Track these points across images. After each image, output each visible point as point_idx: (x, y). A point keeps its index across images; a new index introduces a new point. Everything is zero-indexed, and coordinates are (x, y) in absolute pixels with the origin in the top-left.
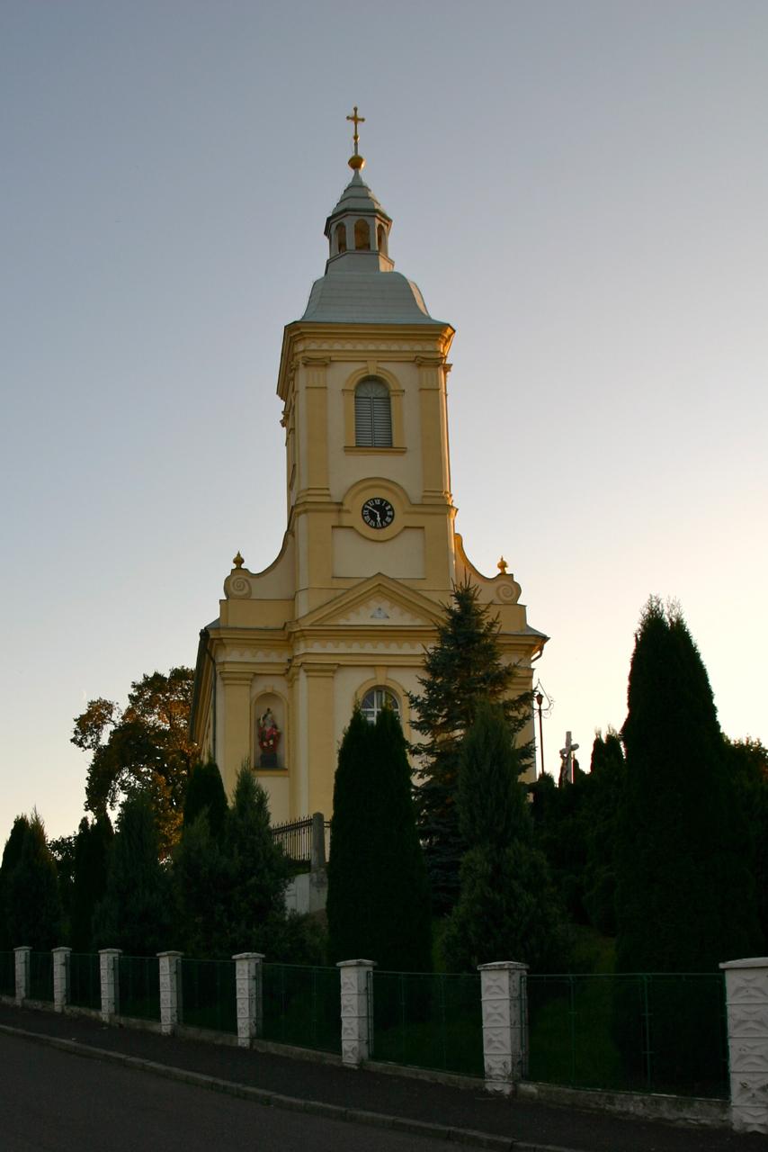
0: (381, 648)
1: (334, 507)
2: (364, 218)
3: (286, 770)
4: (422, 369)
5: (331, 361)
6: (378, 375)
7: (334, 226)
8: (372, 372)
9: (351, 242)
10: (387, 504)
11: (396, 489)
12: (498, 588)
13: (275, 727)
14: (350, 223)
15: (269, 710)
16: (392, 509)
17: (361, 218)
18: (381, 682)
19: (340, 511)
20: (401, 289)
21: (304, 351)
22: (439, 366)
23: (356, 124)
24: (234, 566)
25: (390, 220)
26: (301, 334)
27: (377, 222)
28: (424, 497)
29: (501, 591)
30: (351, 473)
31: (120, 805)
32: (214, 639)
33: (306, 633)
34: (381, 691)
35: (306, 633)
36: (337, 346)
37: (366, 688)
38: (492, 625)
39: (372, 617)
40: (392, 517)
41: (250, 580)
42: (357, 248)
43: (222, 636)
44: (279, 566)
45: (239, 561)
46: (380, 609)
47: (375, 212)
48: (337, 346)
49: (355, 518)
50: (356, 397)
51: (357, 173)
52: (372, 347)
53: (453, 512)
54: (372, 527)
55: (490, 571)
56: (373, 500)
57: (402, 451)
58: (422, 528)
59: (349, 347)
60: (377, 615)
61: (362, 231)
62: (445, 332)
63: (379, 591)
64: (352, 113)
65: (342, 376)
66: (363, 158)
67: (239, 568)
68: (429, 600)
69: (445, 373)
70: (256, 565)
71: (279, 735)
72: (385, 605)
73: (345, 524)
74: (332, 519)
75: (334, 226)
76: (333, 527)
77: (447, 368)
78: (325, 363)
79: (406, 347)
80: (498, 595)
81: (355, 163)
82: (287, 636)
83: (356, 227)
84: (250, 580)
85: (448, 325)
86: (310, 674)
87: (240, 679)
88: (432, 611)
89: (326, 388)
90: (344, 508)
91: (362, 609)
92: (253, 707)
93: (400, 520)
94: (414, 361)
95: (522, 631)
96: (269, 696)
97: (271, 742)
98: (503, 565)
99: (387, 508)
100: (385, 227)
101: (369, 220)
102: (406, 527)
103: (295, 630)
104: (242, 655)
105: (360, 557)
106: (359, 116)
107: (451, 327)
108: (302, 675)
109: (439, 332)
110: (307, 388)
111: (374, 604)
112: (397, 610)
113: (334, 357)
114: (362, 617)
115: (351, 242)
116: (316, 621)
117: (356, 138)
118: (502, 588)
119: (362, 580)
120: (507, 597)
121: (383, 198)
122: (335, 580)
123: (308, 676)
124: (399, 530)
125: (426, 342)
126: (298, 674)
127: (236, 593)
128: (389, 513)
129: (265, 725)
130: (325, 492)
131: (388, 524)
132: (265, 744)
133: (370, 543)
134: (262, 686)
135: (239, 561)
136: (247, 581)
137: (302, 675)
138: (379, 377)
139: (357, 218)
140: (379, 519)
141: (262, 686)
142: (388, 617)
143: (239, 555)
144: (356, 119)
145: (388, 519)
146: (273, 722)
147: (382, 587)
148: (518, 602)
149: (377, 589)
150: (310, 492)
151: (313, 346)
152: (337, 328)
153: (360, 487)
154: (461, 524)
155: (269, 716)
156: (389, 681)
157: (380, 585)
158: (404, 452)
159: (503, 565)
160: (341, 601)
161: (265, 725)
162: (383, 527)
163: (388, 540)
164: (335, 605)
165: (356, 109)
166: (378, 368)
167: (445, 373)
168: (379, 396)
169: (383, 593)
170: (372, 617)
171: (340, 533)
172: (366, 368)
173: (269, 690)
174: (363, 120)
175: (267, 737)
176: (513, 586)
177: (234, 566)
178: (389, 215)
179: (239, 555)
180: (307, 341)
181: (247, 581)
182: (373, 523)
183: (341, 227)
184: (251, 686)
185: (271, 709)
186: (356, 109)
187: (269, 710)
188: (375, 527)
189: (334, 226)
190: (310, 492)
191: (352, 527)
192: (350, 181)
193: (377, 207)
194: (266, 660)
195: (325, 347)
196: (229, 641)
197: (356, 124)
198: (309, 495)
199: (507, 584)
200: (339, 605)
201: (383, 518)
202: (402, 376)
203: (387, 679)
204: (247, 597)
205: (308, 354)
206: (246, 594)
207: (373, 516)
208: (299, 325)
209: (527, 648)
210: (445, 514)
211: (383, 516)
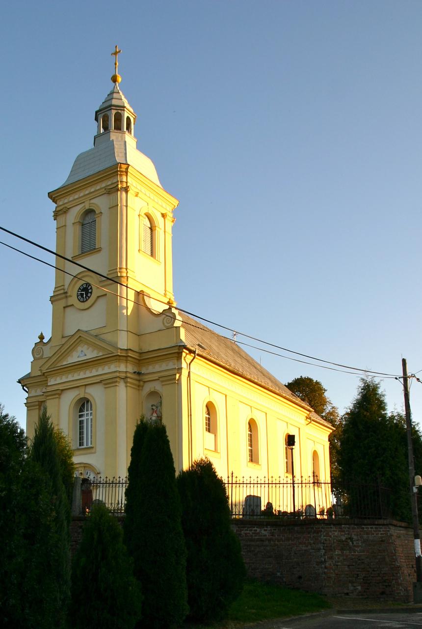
1: (64, 295)
2: (119, 111)
3: (219, 453)
5: (69, 209)
6: (91, 208)
12: (164, 319)
17: (104, 113)
19: (66, 297)
24: (39, 340)
27: (114, 112)
31: (417, 488)
39: (78, 357)
40: (91, 293)
43: (25, 383)
49: (74, 300)
52: (82, 194)
60: (81, 355)
62: (120, 167)
65: (74, 214)
76: (64, 307)
80: (163, 324)
88: (66, 348)
90: (68, 294)
93: (95, 293)
102: (98, 297)
111: (79, 349)
113: (68, 206)
114: (74, 358)
116: (49, 367)
119: (69, 337)
120: (168, 323)
130: (62, 287)
133: (83, 312)
136: (42, 348)
140: (84, 296)
142: (86, 355)
143: (42, 334)
145: (89, 295)
148: (175, 325)
149: (79, 340)
152: (68, 188)
156: (86, 394)
157: (80, 336)
158: (100, 251)
160: (61, 351)
166: (90, 204)
170: (78, 357)
171: (68, 310)
172: (85, 206)
177: (39, 340)
179: (42, 334)
182: (82, 300)
201: (86, 295)
202: (101, 203)
207: (82, 295)
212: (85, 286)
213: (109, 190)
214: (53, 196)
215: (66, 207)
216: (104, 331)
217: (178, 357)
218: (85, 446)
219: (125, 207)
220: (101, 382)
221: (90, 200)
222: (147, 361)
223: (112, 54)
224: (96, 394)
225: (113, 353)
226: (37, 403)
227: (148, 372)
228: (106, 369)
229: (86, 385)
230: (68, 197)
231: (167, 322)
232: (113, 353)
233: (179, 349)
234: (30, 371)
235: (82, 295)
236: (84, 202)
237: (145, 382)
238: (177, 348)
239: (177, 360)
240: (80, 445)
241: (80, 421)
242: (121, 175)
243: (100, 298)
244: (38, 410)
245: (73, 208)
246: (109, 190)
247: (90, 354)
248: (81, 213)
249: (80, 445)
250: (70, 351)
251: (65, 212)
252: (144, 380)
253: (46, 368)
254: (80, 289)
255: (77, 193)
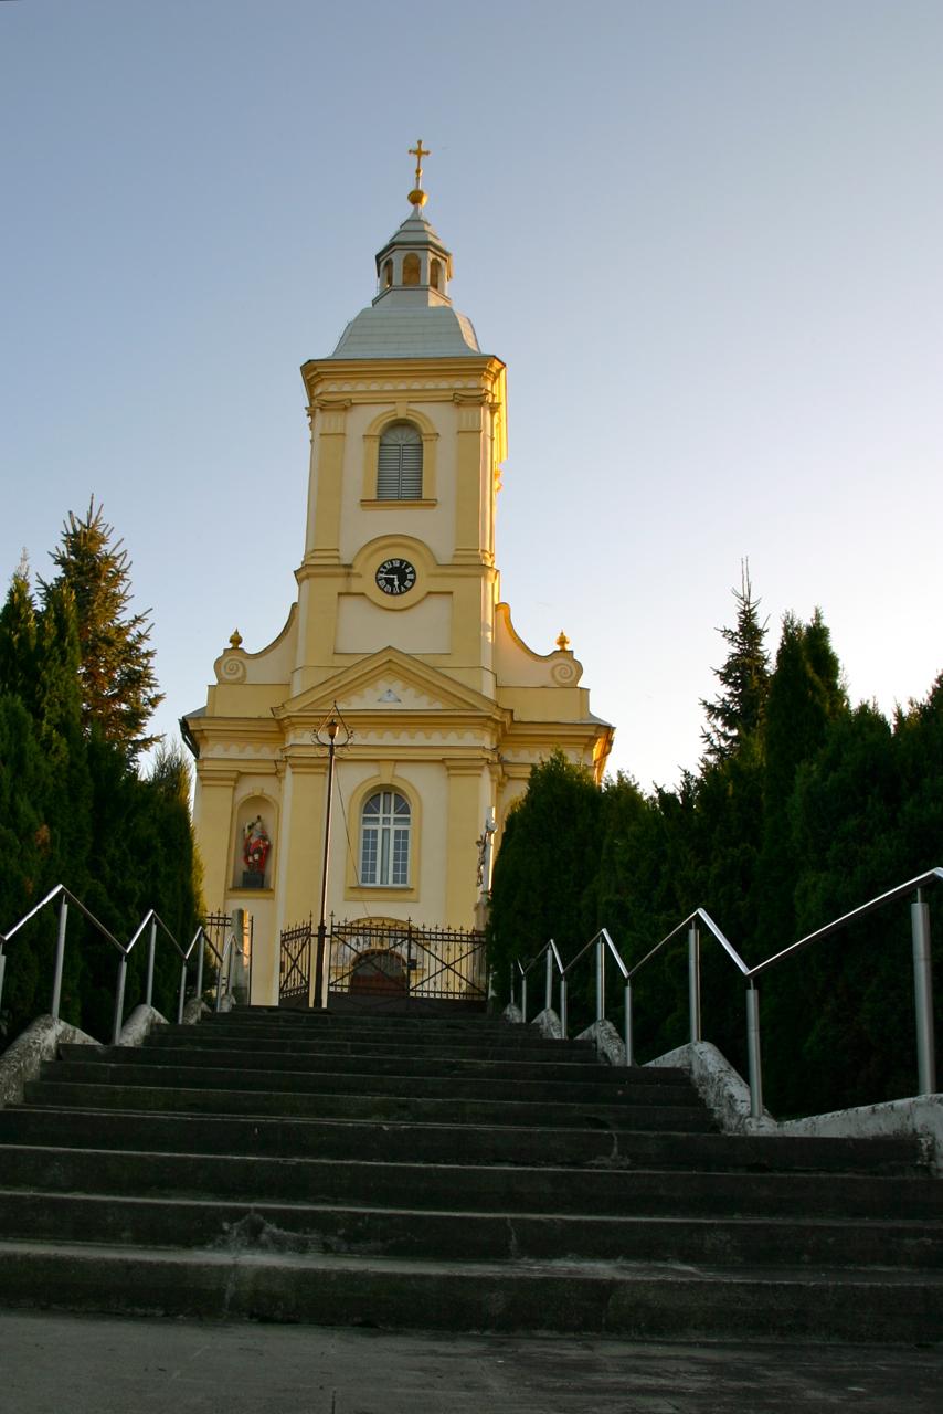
0: (388, 738)
1: (342, 570)
4: (461, 408)
5: (353, 404)
6: (410, 418)
7: (383, 260)
8: (401, 415)
9: (398, 278)
10: (408, 565)
11: (420, 548)
12: (553, 668)
13: (264, 838)
14: (398, 258)
15: (259, 818)
16: (413, 572)
18: (386, 780)
19: (348, 575)
20: (447, 321)
21: (321, 394)
22: (482, 404)
23: (419, 158)
24: (230, 646)
25: (447, 254)
26: (319, 374)
27: (431, 256)
28: (455, 556)
29: (556, 673)
30: (369, 530)
32: (194, 731)
33: (294, 720)
34: (390, 794)
35: (294, 720)
36: (361, 387)
37: (361, 793)
38: (141, 637)
40: (413, 581)
41: (245, 661)
42: (405, 283)
43: (203, 727)
44: (284, 642)
45: (236, 640)
46: (390, 691)
47: (426, 245)
48: (361, 387)
49: (367, 583)
50: (381, 445)
51: (416, 209)
52: (402, 386)
53: (491, 574)
54: (387, 593)
55: (544, 646)
56: (391, 561)
57: (432, 504)
58: (451, 593)
59: (374, 387)
61: (412, 269)
62: (491, 365)
63: (389, 669)
64: (416, 146)
65: (366, 420)
66: (424, 191)
67: (235, 648)
68: (450, 679)
69: (492, 413)
70: (251, 646)
71: (268, 848)
72: (397, 686)
73: (354, 590)
74: (338, 584)
75: (383, 264)
76: (340, 594)
77: (494, 408)
78: (345, 407)
79: (444, 384)
80: (553, 676)
81: (415, 198)
82: (278, 726)
83: (409, 262)
84: (245, 661)
85: (495, 357)
86: (297, 770)
87: (222, 779)
89: (344, 434)
90: (354, 571)
91: (368, 691)
92: (236, 812)
93: (423, 584)
94: (452, 401)
95: (582, 719)
96: (258, 801)
97: (257, 857)
98: (562, 641)
99: (407, 571)
100: (443, 263)
101: (420, 254)
102: (430, 593)
103: (282, 717)
104: (226, 750)
105: (369, 627)
106: (423, 149)
107: (498, 360)
108: (289, 771)
109: (481, 365)
110: (321, 435)
111: (383, 685)
112: (411, 691)
115: (398, 278)
117: (418, 172)
118: (559, 668)
121: (440, 230)
122: (337, 657)
123: (293, 773)
124: (422, 595)
125: (467, 377)
126: (284, 771)
127: (228, 677)
128: (409, 576)
129: (251, 836)
130: (335, 553)
131: (408, 589)
132: (250, 859)
134: (248, 788)
135: (236, 640)
136: (241, 662)
137: (289, 771)
138: (411, 421)
139: (408, 252)
140: (396, 583)
141: (248, 788)
142: (399, 701)
143: (237, 633)
144: (419, 153)
145: (408, 584)
146: (263, 832)
147: (391, 664)
148: (579, 685)
149: (385, 667)
150: (317, 554)
151: (332, 388)
152: (361, 366)
153: (373, 547)
154: (504, 587)
155: (259, 825)
157: (390, 661)
158: (434, 505)
159: (562, 641)
160: (339, 681)
161: (251, 836)
162: (401, 593)
163: (411, 607)
164: (332, 685)
165: (420, 142)
166: (408, 410)
167: (492, 413)
168: (412, 442)
169: (394, 671)
171: (347, 602)
172: (394, 410)
173: (257, 793)
174: (427, 153)
175: (251, 851)
176: (573, 667)
177: (230, 646)
178: (448, 250)
179: (237, 633)
180: (326, 383)
181: (241, 662)
182: (388, 588)
183: (389, 264)
184: (235, 788)
185: (262, 818)
186: (420, 142)
187: (259, 818)
188: (392, 593)
189: (383, 264)
190: (317, 554)
191: (363, 594)
192: (409, 215)
193: (431, 239)
194: (258, 756)
195: (347, 388)
196: (211, 733)
197: (419, 158)
198: (313, 557)
199: (564, 660)
200: (336, 686)
201: (402, 583)
202: (437, 417)
203: (393, 776)
204: (240, 682)
205: (324, 397)
206: (238, 679)
207: (390, 582)
208: (316, 364)
209: (586, 740)
210: (480, 577)
211: (402, 580)
212: (397, 564)
213: (461, 398)
214: (313, 373)
215: (351, 400)
216: (444, 661)
217: (586, 745)
218: (378, 883)
219: (489, 440)
220: (443, 761)
221: (410, 402)
222: (528, 739)
223: (410, 152)
224: (424, 785)
225: (480, 710)
226: (234, 775)
227: (517, 760)
228: (452, 739)
229: (397, 761)
230: (342, 382)
231: (235, 673)
232: (480, 710)
233: (596, 732)
234: (203, 703)
235: (390, 582)
236: (394, 403)
237: (510, 778)
238: (594, 728)
239: (585, 749)
240: (364, 880)
241: (366, 831)
242: (486, 378)
243: (433, 596)
244: (231, 789)
245: (363, 407)
246: (461, 398)
247: (412, 700)
248: (385, 422)
249: (364, 880)
250: (357, 686)
251: (345, 409)
252: (511, 775)
253: (300, 707)
254: (385, 567)
255: (338, 382)
